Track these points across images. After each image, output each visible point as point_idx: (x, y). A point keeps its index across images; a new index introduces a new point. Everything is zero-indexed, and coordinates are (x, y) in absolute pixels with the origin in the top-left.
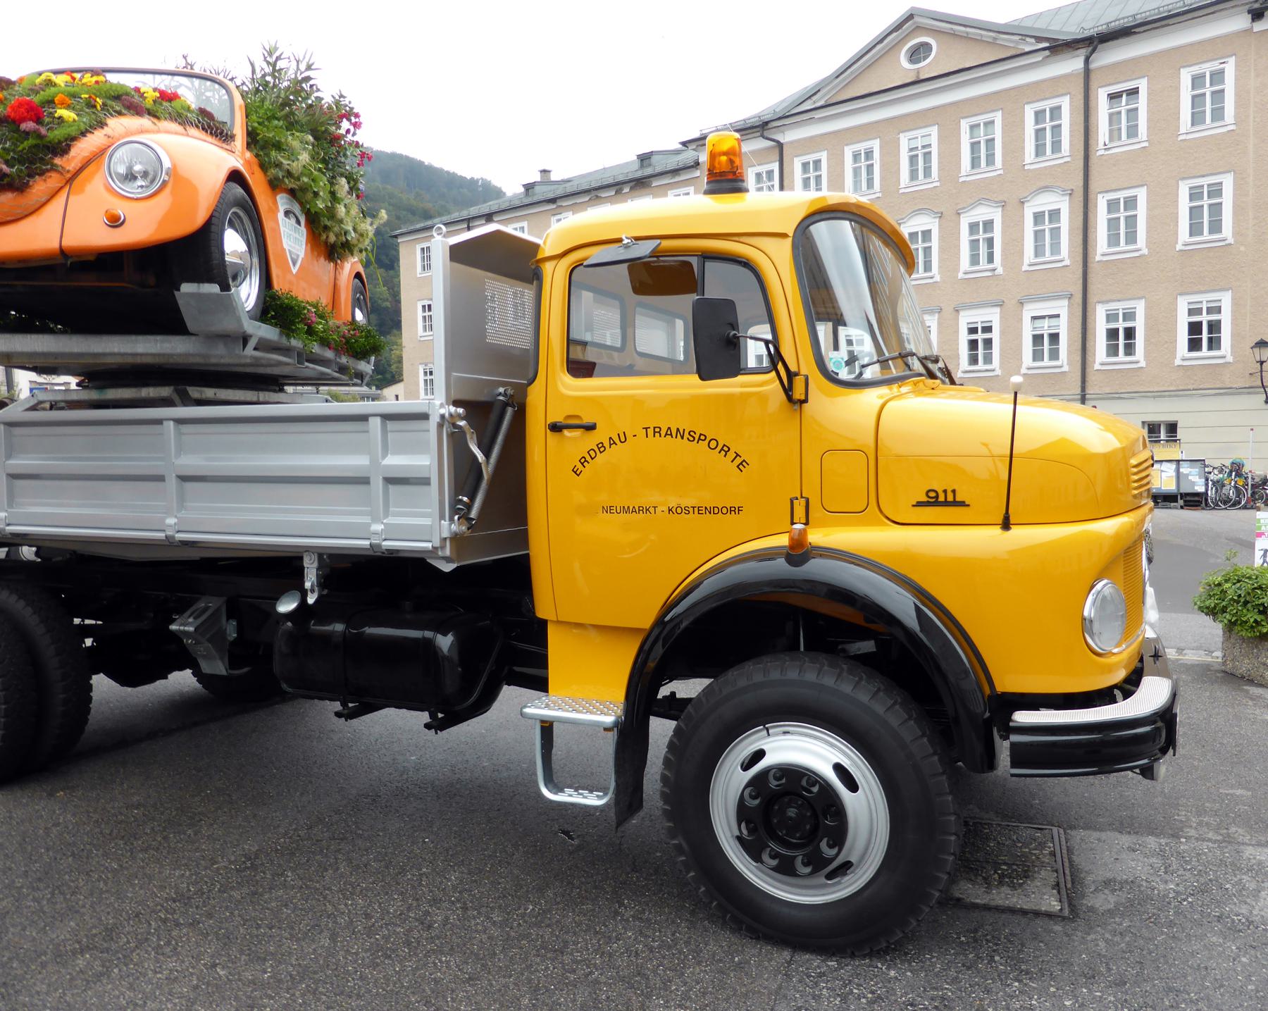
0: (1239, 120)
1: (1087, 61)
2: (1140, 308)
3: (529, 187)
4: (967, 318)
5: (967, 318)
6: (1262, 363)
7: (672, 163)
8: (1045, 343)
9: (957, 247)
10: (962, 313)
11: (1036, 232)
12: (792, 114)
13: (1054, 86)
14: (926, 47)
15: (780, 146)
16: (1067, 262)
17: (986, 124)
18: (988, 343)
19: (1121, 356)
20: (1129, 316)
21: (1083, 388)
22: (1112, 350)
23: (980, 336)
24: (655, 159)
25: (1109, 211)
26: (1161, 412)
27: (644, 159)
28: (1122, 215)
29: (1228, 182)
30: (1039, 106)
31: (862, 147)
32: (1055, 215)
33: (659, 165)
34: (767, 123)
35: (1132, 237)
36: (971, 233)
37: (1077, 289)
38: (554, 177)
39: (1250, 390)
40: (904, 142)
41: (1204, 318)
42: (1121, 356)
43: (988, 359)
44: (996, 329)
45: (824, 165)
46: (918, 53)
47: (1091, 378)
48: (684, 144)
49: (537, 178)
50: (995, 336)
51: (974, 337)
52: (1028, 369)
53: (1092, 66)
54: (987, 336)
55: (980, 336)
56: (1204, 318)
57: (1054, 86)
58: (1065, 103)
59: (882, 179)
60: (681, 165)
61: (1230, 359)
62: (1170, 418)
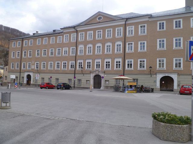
0: (147, 33)
1: (126, 22)
2: (133, 60)
3: (34, 34)
4: (106, 60)
5: (87, 61)
6: (151, 70)
7: (59, 32)
8: (118, 65)
9: (105, 49)
10: (87, 60)
11: (117, 48)
12: (79, 25)
13: (120, 26)
14: (101, 18)
15: (77, 31)
16: (122, 53)
17: (131, 27)
18: (109, 65)
19: (108, 68)
20: (131, 62)
21: (124, 73)
22: (128, 67)
23: (118, 63)
24: (56, 31)
25: (140, 44)
26: (135, 77)
27: (54, 31)
28: (178, 42)
29: (146, 42)
30: (81, 33)
31: (82, 33)
32: (120, 45)
33: (57, 32)
34: (75, 27)
35: (180, 46)
36: (107, 47)
37: (123, 57)
38: (39, 33)
39: (148, 74)
40: (88, 33)
41: (130, 63)
42: (108, 68)
43: (109, 67)
44: (100, 63)
45: (84, 34)
46: (99, 19)
47: (125, 71)
48: (61, 29)
49: (36, 32)
50: (110, 64)
51: (160, 62)
52: (6, 71)
53: (126, 23)
54: (163, 62)
55: (108, 64)
56: (72, 64)
57: (120, 26)
58: (122, 28)
59: (93, 37)
60: (60, 32)
61: (146, 69)
62: (137, 78)
